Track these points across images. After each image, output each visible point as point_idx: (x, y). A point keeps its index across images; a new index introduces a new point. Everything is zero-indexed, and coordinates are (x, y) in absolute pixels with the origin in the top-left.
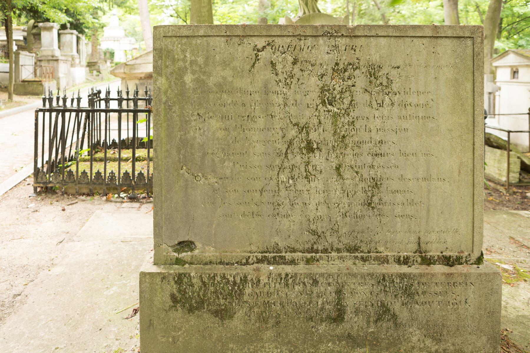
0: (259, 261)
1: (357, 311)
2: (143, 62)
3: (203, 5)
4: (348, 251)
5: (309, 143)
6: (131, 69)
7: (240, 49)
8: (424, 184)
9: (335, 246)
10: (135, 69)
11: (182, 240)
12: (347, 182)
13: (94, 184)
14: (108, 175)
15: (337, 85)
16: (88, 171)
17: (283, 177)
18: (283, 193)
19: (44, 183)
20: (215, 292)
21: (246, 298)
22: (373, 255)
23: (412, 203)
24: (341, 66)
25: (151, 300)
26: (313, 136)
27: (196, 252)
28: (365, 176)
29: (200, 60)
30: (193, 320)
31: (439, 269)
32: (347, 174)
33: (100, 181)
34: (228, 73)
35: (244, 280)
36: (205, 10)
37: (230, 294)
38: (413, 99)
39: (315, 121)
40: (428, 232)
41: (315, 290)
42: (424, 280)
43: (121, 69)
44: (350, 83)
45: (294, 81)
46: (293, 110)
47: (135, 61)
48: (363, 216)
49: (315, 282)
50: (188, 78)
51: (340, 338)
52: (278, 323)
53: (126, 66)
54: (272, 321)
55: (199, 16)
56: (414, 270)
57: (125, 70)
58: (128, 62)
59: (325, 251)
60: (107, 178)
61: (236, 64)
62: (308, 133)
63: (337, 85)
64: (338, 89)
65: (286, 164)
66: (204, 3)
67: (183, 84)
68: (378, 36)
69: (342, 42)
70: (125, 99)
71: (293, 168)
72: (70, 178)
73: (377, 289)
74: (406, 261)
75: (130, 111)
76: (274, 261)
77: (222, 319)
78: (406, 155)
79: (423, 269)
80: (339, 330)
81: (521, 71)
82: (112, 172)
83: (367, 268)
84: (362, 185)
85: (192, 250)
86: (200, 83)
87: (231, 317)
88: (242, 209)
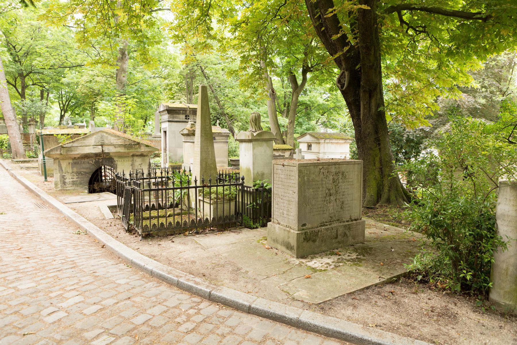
0: (320, 226)
2: (80, 145)
5: (330, 193)
6: (68, 151)
10: (72, 151)
13: (177, 228)
15: (336, 178)
16: (156, 223)
17: (325, 203)
18: (325, 207)
19: (147, 232)
23: (349, 207)
26: (331, 192)
31: (354, 222)
33: (179, 226)
35: (319, 231)
38: (350, 180)
43: (57, 151)
46: (327, 185)
47: (71, 144)
50: (306, 178)
51: (337, 242)
53: (62, 149)
55: (205, 131)
56: (350, 223)
57: (62, 151)
58: (65, 144)
59: (333, 221)
61: (316, 173)
67: (305, 180)
69: (337, 166)
71: (327, 200)
72: (162, 227)
74: (348, 221)
76: (324, 225)
80: (337, 240)
81: (313, 146)
82: (185, 221)
83: (342, 224)
86: (308, 179)
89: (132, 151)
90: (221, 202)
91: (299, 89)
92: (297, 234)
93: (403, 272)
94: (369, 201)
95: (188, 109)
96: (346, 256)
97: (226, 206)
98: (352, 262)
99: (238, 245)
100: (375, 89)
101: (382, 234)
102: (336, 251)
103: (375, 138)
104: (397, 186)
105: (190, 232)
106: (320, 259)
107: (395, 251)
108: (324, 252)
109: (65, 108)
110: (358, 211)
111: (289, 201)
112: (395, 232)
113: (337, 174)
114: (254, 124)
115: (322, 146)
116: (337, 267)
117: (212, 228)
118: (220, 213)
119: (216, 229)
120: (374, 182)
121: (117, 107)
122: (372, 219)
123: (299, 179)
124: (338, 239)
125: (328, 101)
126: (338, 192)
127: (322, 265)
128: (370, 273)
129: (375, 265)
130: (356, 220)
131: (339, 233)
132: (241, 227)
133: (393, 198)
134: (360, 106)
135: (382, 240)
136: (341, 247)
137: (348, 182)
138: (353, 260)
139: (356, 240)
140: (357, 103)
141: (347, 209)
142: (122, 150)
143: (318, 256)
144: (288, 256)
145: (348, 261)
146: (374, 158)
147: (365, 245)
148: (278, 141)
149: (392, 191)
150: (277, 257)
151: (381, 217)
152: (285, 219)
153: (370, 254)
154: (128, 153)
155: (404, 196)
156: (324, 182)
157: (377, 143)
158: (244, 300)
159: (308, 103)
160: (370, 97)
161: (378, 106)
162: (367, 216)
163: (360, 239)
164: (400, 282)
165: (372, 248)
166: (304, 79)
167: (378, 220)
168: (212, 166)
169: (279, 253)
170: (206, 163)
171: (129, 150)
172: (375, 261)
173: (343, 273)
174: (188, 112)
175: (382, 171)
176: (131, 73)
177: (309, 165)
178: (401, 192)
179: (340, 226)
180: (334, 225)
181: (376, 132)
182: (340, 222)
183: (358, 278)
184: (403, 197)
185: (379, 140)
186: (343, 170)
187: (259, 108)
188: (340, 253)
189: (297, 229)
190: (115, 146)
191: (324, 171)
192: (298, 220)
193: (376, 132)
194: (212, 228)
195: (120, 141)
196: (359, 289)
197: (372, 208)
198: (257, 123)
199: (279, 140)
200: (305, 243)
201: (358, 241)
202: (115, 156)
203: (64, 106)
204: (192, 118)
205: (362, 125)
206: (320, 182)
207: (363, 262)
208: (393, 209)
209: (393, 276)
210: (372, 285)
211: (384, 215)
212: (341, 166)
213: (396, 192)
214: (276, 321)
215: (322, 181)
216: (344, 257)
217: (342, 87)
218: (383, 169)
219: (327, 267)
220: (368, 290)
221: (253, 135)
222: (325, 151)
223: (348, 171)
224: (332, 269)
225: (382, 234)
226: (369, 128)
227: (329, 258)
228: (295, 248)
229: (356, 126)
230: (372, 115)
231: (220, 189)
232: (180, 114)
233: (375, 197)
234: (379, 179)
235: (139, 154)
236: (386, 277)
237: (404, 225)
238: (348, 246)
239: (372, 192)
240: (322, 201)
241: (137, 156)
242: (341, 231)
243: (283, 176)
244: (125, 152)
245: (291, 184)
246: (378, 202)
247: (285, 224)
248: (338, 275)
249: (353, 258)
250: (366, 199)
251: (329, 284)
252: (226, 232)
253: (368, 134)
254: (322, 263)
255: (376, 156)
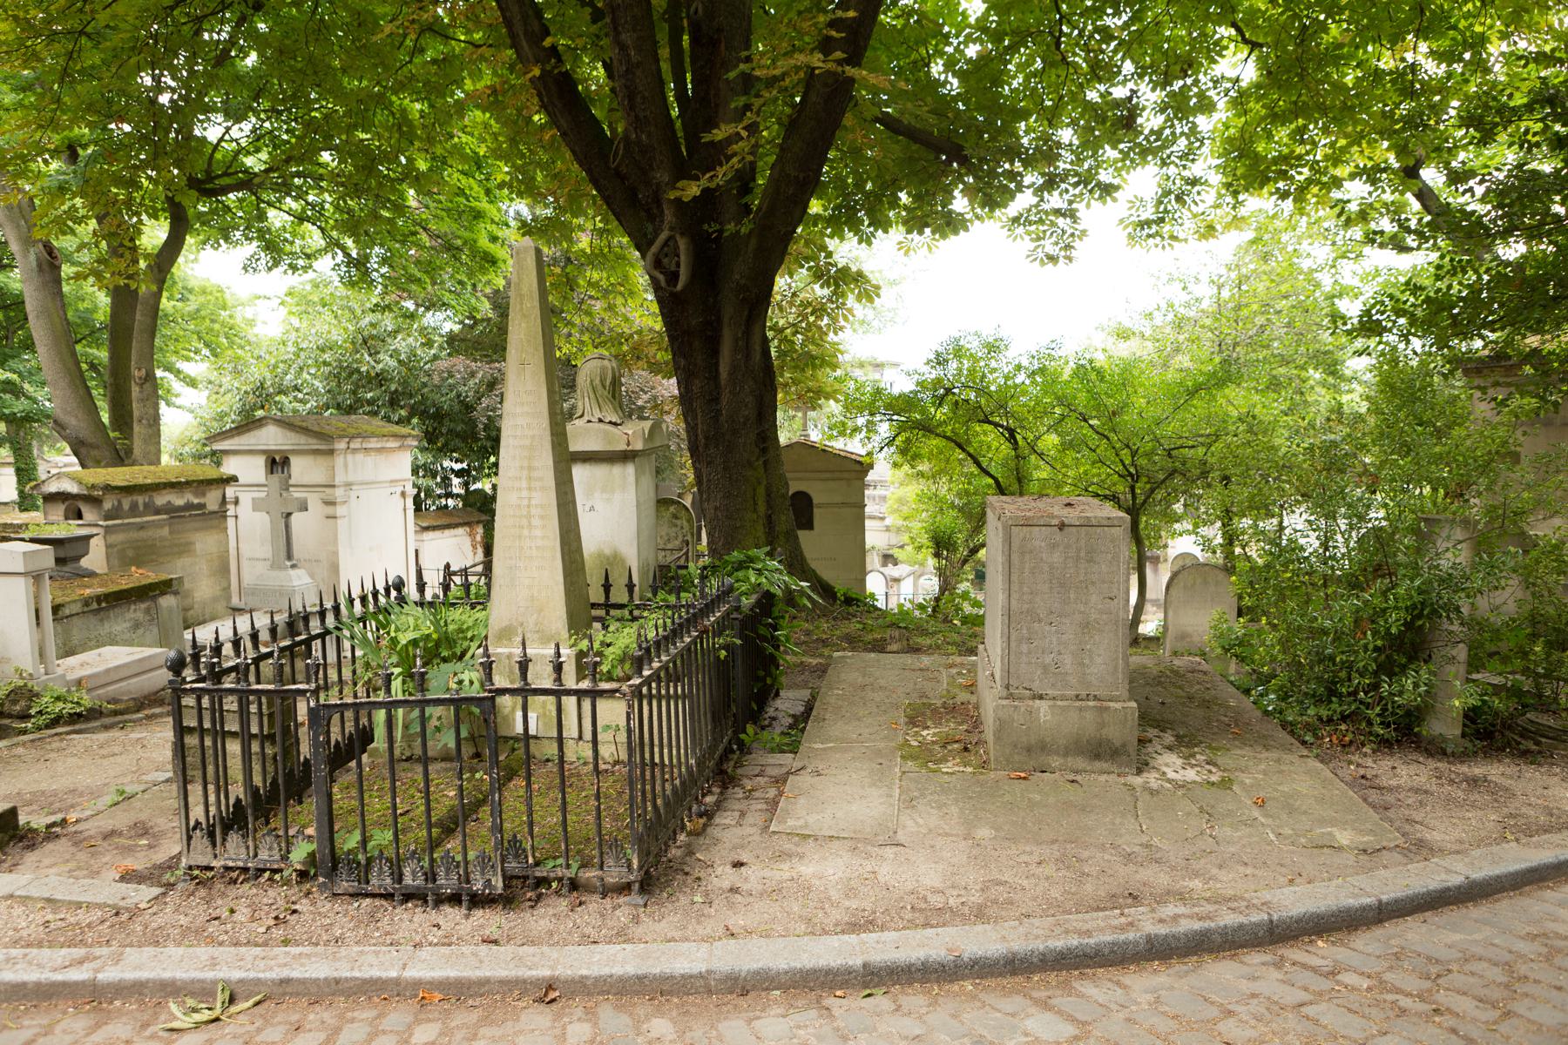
115: (339, 460)
148: (95, 453)
158: (1355, 896)
199: (98, 447)
214: (1462, 902)
222: (351, 478)
255: (759, 483)
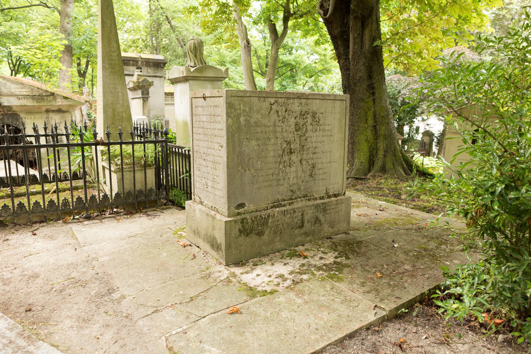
0: (272, 207)
1: (308, 222)
3: (113, 49)
4: (304, 197)
5: (291, 149)
7: (264, 103)
8: (329, 164)
9: (299, 196)
11: (239, 203)
12: (304, 166)
14: (61, 202)
15: (301, 122)
17: (281, 167)
18: (281, 174)
20: (257, 224)
21: (269, 224)
22: (312, 197)
23: (325, 173)
24: (303, 113)
25: (230, 234)
27: (246, 208)
28: (310, 163)
29: (247, 109)
30: (248, 239)
31: (333, 199)
32: (304, 163)
33: (54, 208)
34: (259, 116)
35: (269, 216)
36: (115, 54)
37: (263, 224)
38: (327, 128)
39: (293, 139)
40: (330, 185)
41: (295, 215)
42: (329, 204)
44: (306, 121)
45: (286, 120)
46: (285, 134)
48: (309, 181)
49: (295, 212)
50: (242, 119)
51: (302, 234)
52: (281, 233)
54: (279, 233)
55: (109, 60)
56: (326, 200)
59: (296, 199)
60: (61, 204)
61: (263, 111)
62: (290, 145)
63: (301, 122)
64: (302, 124)
65: (282, 161)
66: (113, 48)
67: (240, 122)
68: (316, 99)
69: (304, 101)
70: (43, 136)
71: (285, 162)
72: (21, 209)
73: (315, 211)
74: (322, 198)
75: (50, 146)
76: (280, 206)
77: (260, 236)
78: (324, 152)
79: (328, 200)
80: (302, 231)
82: (65, 199)
83: (311, 203)
84: (309, 167)
85: (243, 208)
87: (263, 234)
88: (265, 184)
89: (45, 105)
90: (131, 169)
91: (279, 40)
92: (226, 222)
93: (418, 293)
94: (358, 170)
95: (140, 59)
96: (317, 258)
97: (139, 175)
98: (325, 271)
99: (139, 239)
100: (370, 15)
101: (376, 216)
102: (301, 248)
103: (368, 85)
104: (395, 150)
105: (77, 217)
106: (268, 267)
107: (400, 248)
108: (279, 252)
109: (16, 68)
110: (340, 182)
111: (214, 162)
112: (396, 213)
113: (303, 115)
114: (193, 56)
116: (298, 283)
117: (115, 210)
118: (128, 186)
119: (122, 210)
120: (365, 145)
121: (38, 51)
122: (362, 194)
123: (227, 121)
124: (304, 228)
125: (315, 63)
126: (305, 148)
127: (270, 279)
128: (358, 296)
129: (366, 278)
130: (335, 196)
131: (306, 218)
132: (165, 207)
133: (389, 165)
134: (349, 41)
135: (377, 227)
136: (310, 241)
137: (324, 130)
138: (328, 268)
139: (336, 229)
140: (345, 37)
141: (321, 177)
142: (29, 103)
143: (265, 259)
144: (212, 262)
145: (319, 269)
146: (366, 113)
147: (350, 237)
149: (389, 156)
150: (193, 263)
151: (374, 191)
152: (211, 195)
153: (358, 253)
154: (39, 107)
155: (404, 163)
156: (279, 129)
157: (371, 92)
159: (293, 63)
160: (363, 27)
161: (374, 39)
162: (355, 190)
163: (343, 226)
164: (414, 314)
165: (361, 242)
166: (286, 27)
167: (369, 195)
168: (124, 115)
169: (200, 255)
170: (114, 110)
171: (40, 102)
172: (367, 268)
173: (306, 297)
174: (140, 63)
175: (376, 130)
176: (76, 18)
177: (248, 95)
178: (400, 158)
179: (307, 206)
180: (299, 204)
181: (370, 77)
182: (309, 200)
183: (334, 310)
184: (402, 164)
185: (373, 88)
186: (315, 109)
187: (236, 68)
188: (306, 253)
189: (226, 214)
190: (18, 97)
191: (279, 108)
192: (229, 197)
193: (370, 77)
194: (115, 210)
195: (26, 90)
196: (333, 339)
197: (361, 179)
198: (198, 54)
200: (242, 238)
201: (339, 230)
202: (22, 112)
203: (14, 66)
204: (146, 71)
205: (352, 67)
206: (271, 128)
207: (346, 270)
208: (389, 180)
209: (400, 302)
210: (361, 329)
211: (377, 188)
212: (310, 101)
213: (393, 158)
215: (275, 126)
216: (313, 262)
217: (325, 14)
218: (378, 127)
219: (278, 284)
220: (352, 341)
221: (190, 70)
223: (322, 111)
224: (287, 287)
225: (376, 216)
226: (360, 71)
227: (285, 264)
228: (223, 248)
229: (343, 70)
230: (364, 53)
231: (128, 149)
232: (129, 65)
233: (366, 165)
234: (372, 140)
235: (56, 108)
236: (389, 306)
237: (405, 201)
238: (322, 239)
239: (362, 157)
240: (276, 162)
241: (53, 111)
242: (309, 214)
243: (204, 118)
244: (34, 106)
245: (216, 132)
246: (369, 171)
247: (210, 204)
248: (295, 303)
249: (328, 262)
250: (354, 167)
251: (272, 330)
252: (138, 215)
253: (359, 80)
254: (270, 276)
255: (369, 110)
